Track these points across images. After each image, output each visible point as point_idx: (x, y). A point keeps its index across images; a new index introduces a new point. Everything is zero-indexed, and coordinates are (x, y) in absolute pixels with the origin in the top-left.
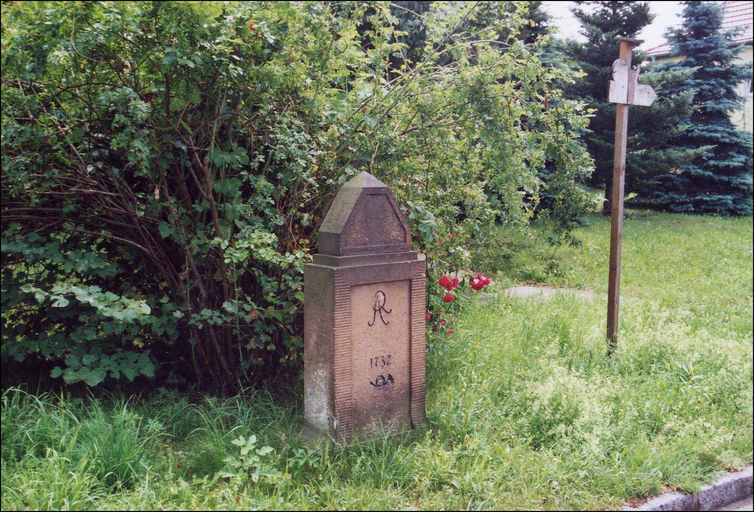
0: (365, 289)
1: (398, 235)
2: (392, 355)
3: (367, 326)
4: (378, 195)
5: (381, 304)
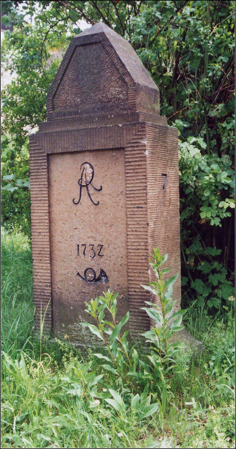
0: (68, 159)
1: (121, 92)
2: (105, 246)
3: (72, 204)
4: (91, 44)
5: (89, 179)
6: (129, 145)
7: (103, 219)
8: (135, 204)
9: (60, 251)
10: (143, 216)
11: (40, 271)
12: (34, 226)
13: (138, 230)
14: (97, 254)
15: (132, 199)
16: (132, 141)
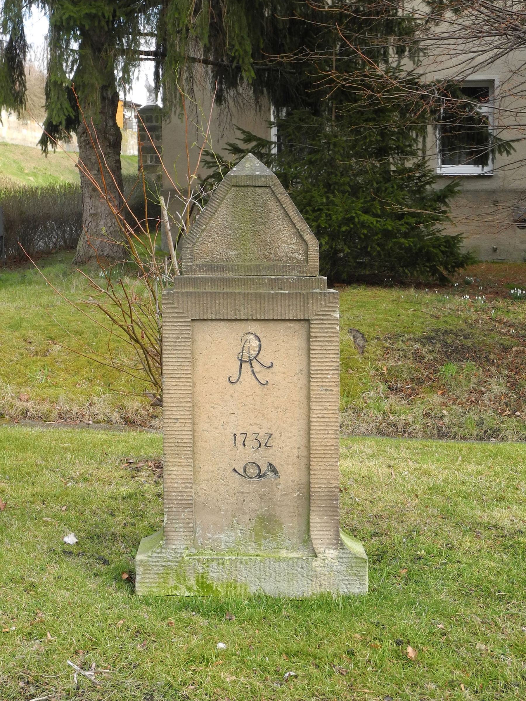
2: (276, 434)
5: (253, 353)
6: (317, 317)
7: (273, 403)
8: (322, 386)
9: (206, 442)
10: (334, 400)
11: (175, 468)
12: (167, 410)
13: (326, 416)
14: (263, 445)
15: (319, 380)
16: (322, 313)
